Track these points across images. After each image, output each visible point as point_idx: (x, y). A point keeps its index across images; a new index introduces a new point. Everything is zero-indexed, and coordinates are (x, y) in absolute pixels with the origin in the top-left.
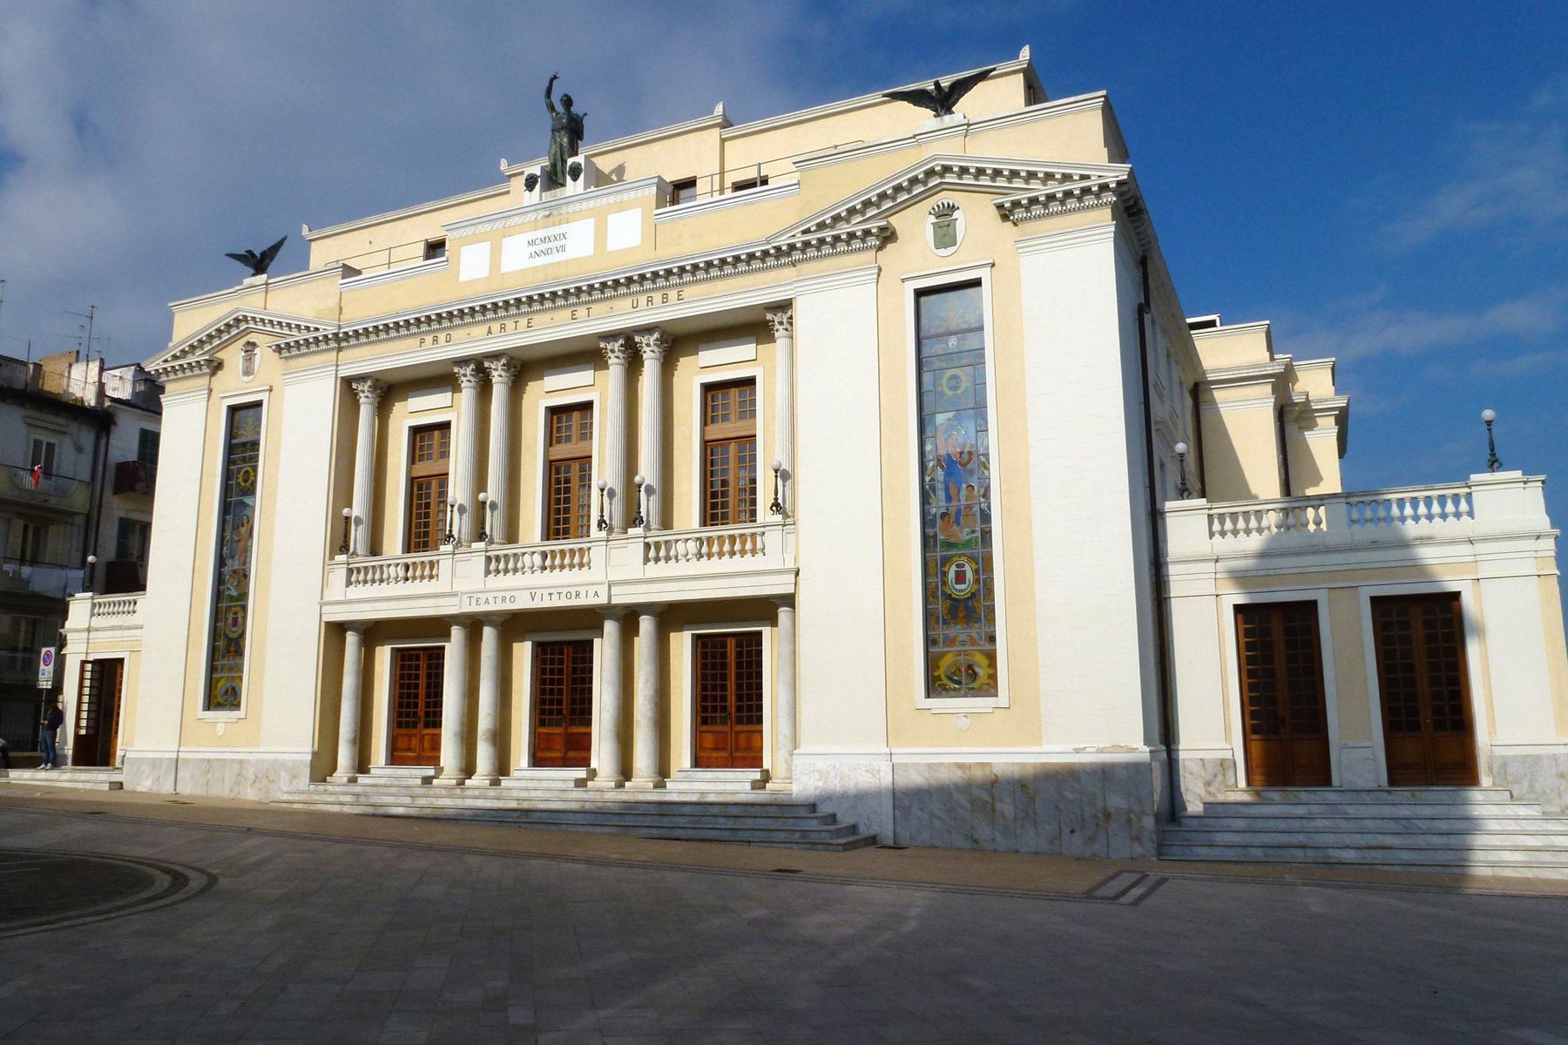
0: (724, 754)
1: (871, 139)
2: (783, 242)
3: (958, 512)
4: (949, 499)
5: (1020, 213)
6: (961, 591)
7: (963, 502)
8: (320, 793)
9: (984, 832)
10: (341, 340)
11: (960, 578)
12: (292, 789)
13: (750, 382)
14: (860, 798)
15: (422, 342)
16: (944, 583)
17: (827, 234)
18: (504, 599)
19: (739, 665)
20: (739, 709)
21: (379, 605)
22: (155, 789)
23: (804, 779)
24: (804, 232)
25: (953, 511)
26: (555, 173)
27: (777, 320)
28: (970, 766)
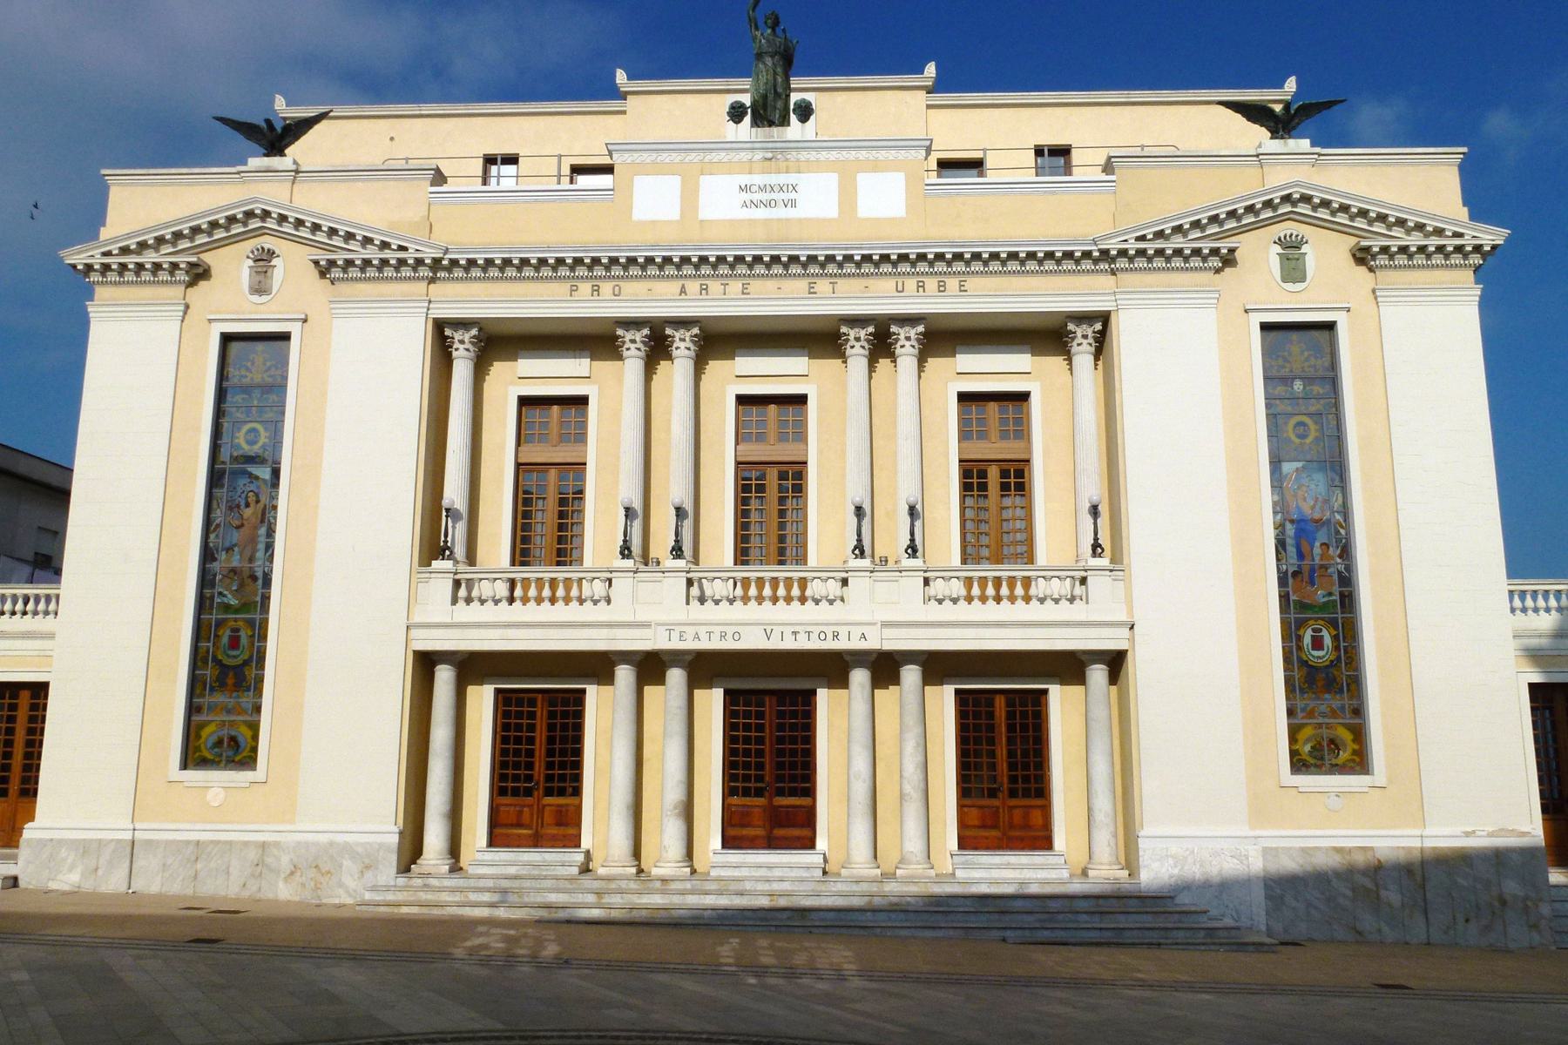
0: (994, 833)
1: (1187, 146)
2: (1113, 246)
3: (1312, 570)
4: (1301, 556)
5: (336, 273)
6: (1321, 656)
7: (1317, 560)
8: (417, 889)
9: (1368, 922)
10: (440, 268)
11: (1317, 643)
12: (364, 885)
13: (582, 401)
14: (1224, 888)
15: (574, 289)
16: (1300, 648)
17: (130, 260)
18: (723, 636)
19: (1011, 728)
20: (1013, 779)
21: (510, 633)
22: (88, 886)
23: (1155, 865)
24: (1139, 239)
25: (1306, 569)
26: (765, 106)
27: (677, 335)
28: (1350, 850)
